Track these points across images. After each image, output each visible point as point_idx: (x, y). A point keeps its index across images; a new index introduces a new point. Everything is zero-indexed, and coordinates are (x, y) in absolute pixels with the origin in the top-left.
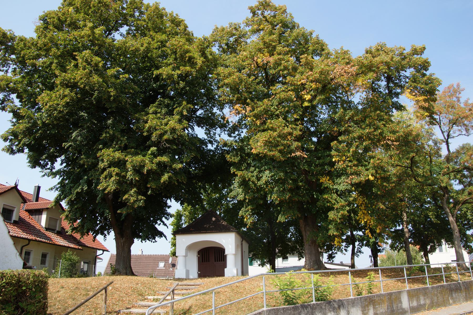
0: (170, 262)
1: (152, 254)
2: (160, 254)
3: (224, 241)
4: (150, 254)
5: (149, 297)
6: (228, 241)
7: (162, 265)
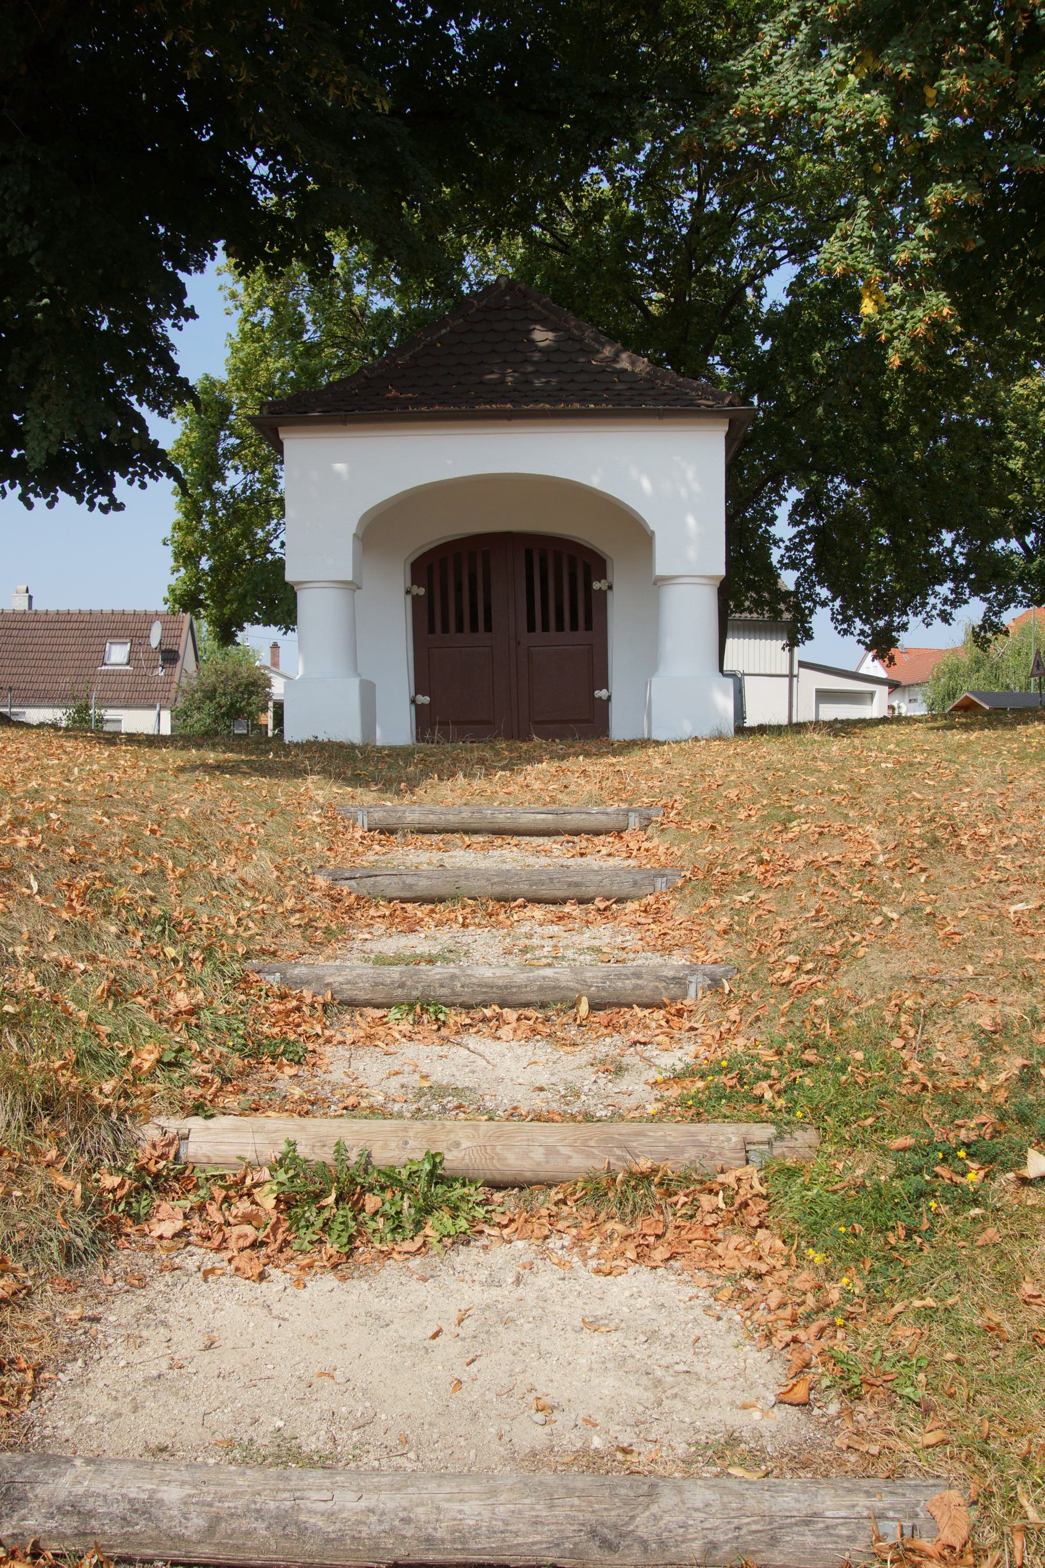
0: (154, 642)
1: (74, 608)
2: (107, 608)
3: (646, 484)
4: (63, 608)
5: (34, 715)
6: (665, 482)
7: (118, 654)
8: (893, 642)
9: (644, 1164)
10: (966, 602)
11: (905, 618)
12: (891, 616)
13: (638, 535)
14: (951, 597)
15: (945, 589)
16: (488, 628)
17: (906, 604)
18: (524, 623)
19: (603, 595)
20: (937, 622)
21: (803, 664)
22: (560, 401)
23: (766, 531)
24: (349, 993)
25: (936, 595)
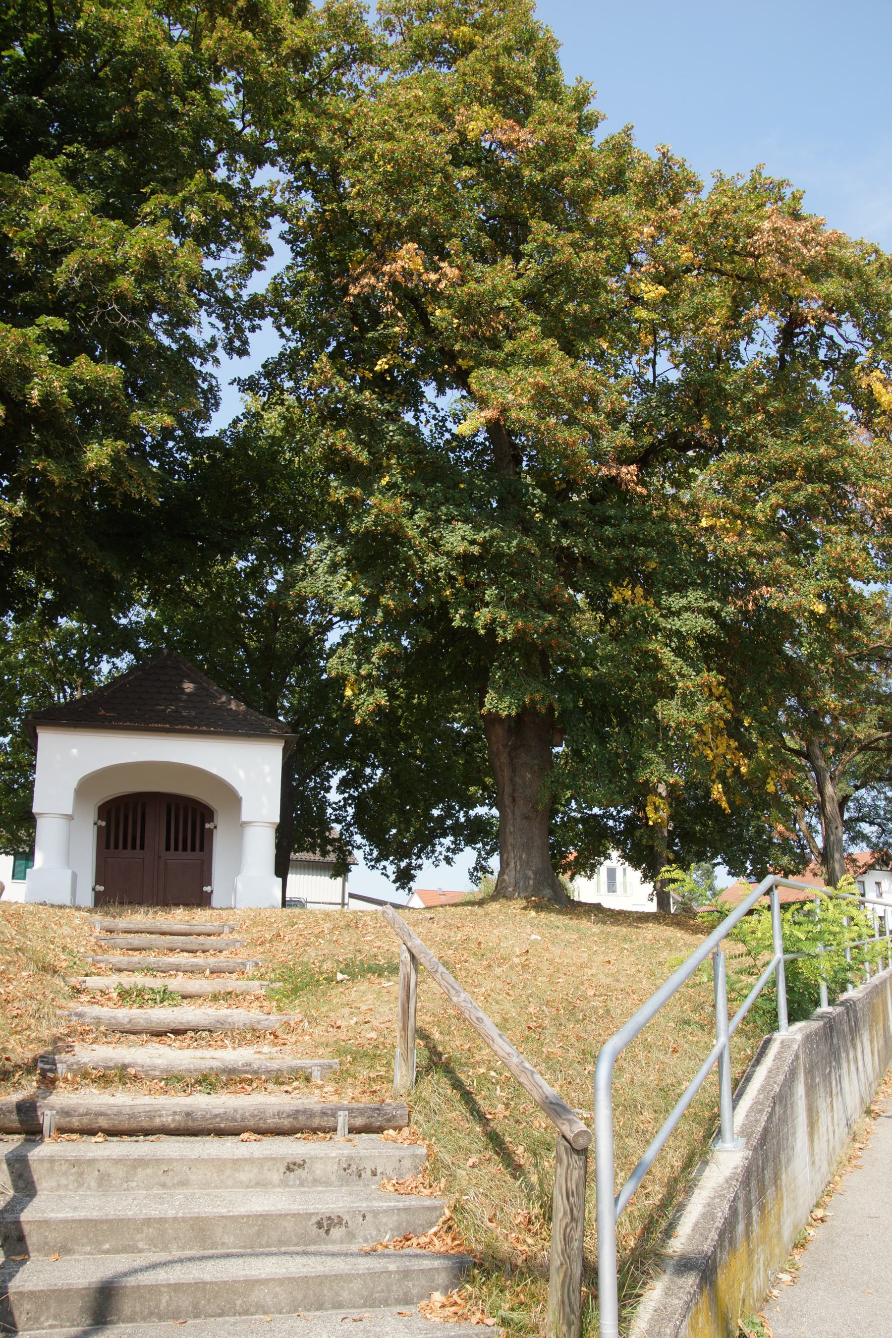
3: (242, 774)
6: (250, 772)
8: (412, 878)
9: (230, 990)
10: (462, 850)
11: (420, 861)
12: (410, 858)
13: (233, 799)
14: (452, 847)
15: (448, 841)
16: (142, 848)
17: (421, 851)
18: (164, 846)
19: (211, 831)
20: (443, 863)
21: (351, 896)
22: (195, 725)
23: (324, 797)
24: (119, 966)
25: (441, 844)
